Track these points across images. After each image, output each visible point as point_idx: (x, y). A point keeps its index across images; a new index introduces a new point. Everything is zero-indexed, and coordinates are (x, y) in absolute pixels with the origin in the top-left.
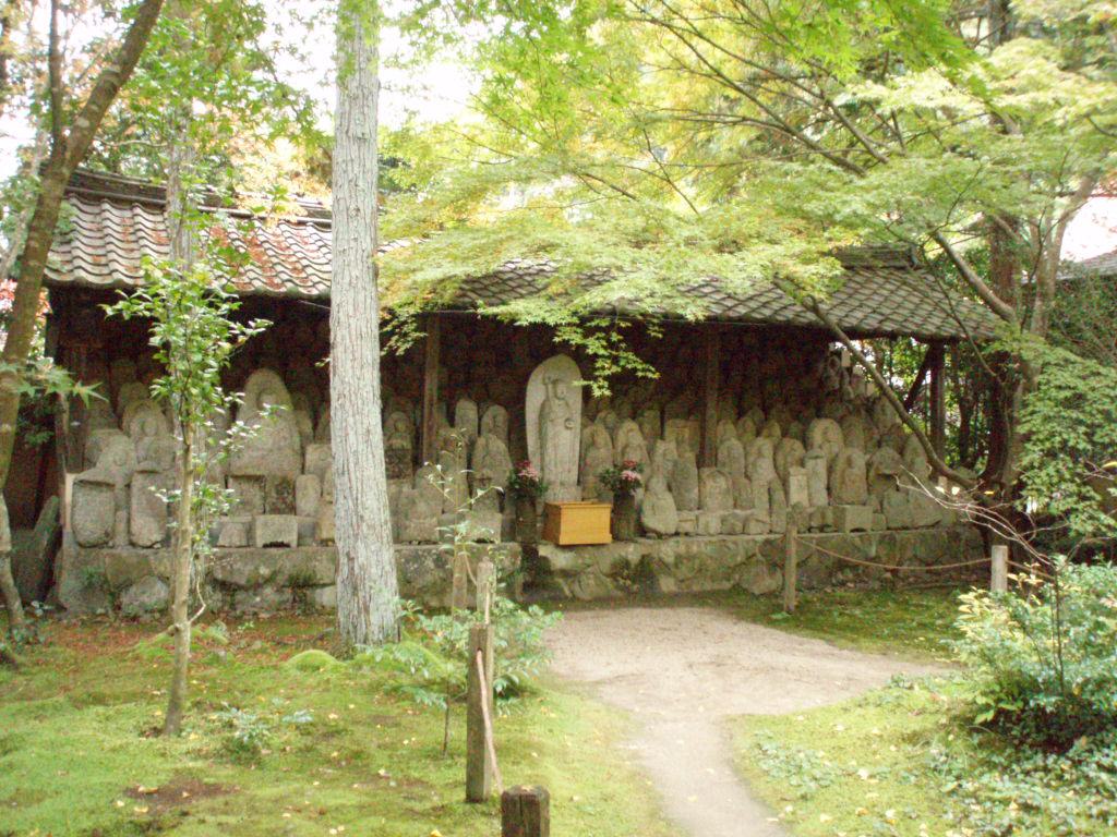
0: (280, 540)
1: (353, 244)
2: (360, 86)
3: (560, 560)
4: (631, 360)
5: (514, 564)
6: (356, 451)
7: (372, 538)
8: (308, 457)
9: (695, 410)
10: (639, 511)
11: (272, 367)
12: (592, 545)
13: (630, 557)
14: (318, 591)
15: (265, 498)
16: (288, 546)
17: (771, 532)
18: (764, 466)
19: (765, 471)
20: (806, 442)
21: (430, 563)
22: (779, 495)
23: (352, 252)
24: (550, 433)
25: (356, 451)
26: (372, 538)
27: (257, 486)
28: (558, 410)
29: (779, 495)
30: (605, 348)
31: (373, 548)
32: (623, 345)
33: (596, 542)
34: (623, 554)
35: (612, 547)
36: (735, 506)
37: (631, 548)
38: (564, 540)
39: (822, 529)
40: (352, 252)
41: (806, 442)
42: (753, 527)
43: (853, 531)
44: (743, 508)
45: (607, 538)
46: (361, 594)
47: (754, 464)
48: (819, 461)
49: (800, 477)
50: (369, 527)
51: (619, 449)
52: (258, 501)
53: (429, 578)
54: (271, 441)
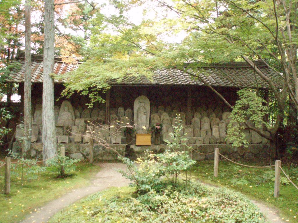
0: (64, 142)
1: (46, 73)
2: (120, 23)
3: (137, 149)
4: (99, 99)
5: (123, 149)
6: (46, 121)
7: (49, 141)
8: (76, 122)
9: (186, 111)
10: (162, 137)
11: (144, 95)
12: (146, 146)
13: (157, 149)
14: (72, 154)
15: (63, 131)
16: (66, 143)
17: (204, 143)
18: (206, 125)
19: (206, 126)
20: (221, 119)
21: (101, 148)
22: (210, 133)
23: (46, 75)
24: (140, 115)
25: (46, 121)
26: (49, 141)
27: (61, 129)
28: (142, 110)
29: (210, 133)
30: (94, 96)
31: (49, 143)
32: (98, 95)
33: (147, 144)
34: (155, 148)
35: (152, 146)
36: (194, 136)
37: (158, 146)
38: (137, 144)
39: (220, 143)
40: (46, 75)
41: (221, 119)
42: (197, 142)
43: (229, 144)
44: (196, 137)
45: (150, 143)
46: (46, 153)
47: (203, 125)
48: (223, 124)
49: (216, 128)
50: (48, 138)
51: (161, 121)
52: (61, 132)
53: (100, 152)
54: (66, 118)
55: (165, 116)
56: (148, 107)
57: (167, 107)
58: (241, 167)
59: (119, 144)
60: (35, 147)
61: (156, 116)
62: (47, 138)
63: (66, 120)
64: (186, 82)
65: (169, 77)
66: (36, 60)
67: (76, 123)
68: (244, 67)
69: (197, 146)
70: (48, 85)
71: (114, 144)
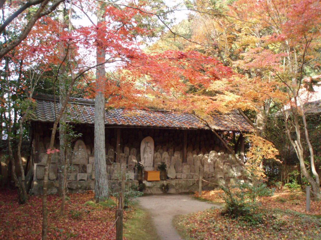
8: (90, 160)
12: (156, 181)
15: (79, 169)
16: (85, 180)
35: (160, 181)
36: (191, 172)
37: (165, 181)
45: (159, 179)
52: (78, 170)
55: (166, 155)
56: (153, 147)
57: (158, 146)
58: (118, 205)
59: (132, 180)
60: (56, 185)
61: (158, 154)
62: (101, 175)
63: (81, 158)
64: (91, 121)
65: (89, 115)
66: (45, 100)
67: (89, 161)
68: (39, 98)
69: (195, 180)
70: (101, 126)
71: (79, 180)
